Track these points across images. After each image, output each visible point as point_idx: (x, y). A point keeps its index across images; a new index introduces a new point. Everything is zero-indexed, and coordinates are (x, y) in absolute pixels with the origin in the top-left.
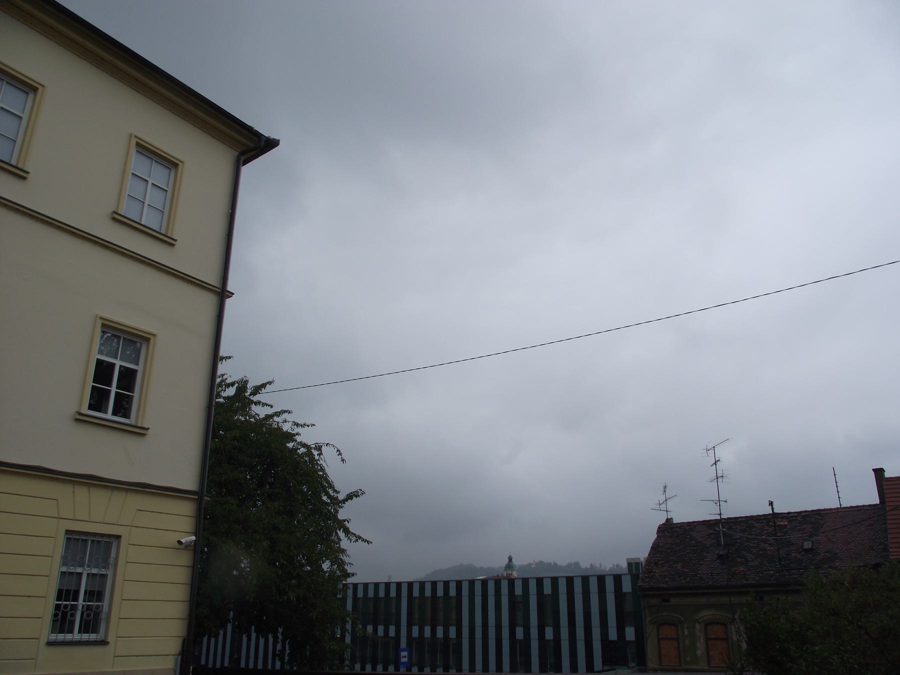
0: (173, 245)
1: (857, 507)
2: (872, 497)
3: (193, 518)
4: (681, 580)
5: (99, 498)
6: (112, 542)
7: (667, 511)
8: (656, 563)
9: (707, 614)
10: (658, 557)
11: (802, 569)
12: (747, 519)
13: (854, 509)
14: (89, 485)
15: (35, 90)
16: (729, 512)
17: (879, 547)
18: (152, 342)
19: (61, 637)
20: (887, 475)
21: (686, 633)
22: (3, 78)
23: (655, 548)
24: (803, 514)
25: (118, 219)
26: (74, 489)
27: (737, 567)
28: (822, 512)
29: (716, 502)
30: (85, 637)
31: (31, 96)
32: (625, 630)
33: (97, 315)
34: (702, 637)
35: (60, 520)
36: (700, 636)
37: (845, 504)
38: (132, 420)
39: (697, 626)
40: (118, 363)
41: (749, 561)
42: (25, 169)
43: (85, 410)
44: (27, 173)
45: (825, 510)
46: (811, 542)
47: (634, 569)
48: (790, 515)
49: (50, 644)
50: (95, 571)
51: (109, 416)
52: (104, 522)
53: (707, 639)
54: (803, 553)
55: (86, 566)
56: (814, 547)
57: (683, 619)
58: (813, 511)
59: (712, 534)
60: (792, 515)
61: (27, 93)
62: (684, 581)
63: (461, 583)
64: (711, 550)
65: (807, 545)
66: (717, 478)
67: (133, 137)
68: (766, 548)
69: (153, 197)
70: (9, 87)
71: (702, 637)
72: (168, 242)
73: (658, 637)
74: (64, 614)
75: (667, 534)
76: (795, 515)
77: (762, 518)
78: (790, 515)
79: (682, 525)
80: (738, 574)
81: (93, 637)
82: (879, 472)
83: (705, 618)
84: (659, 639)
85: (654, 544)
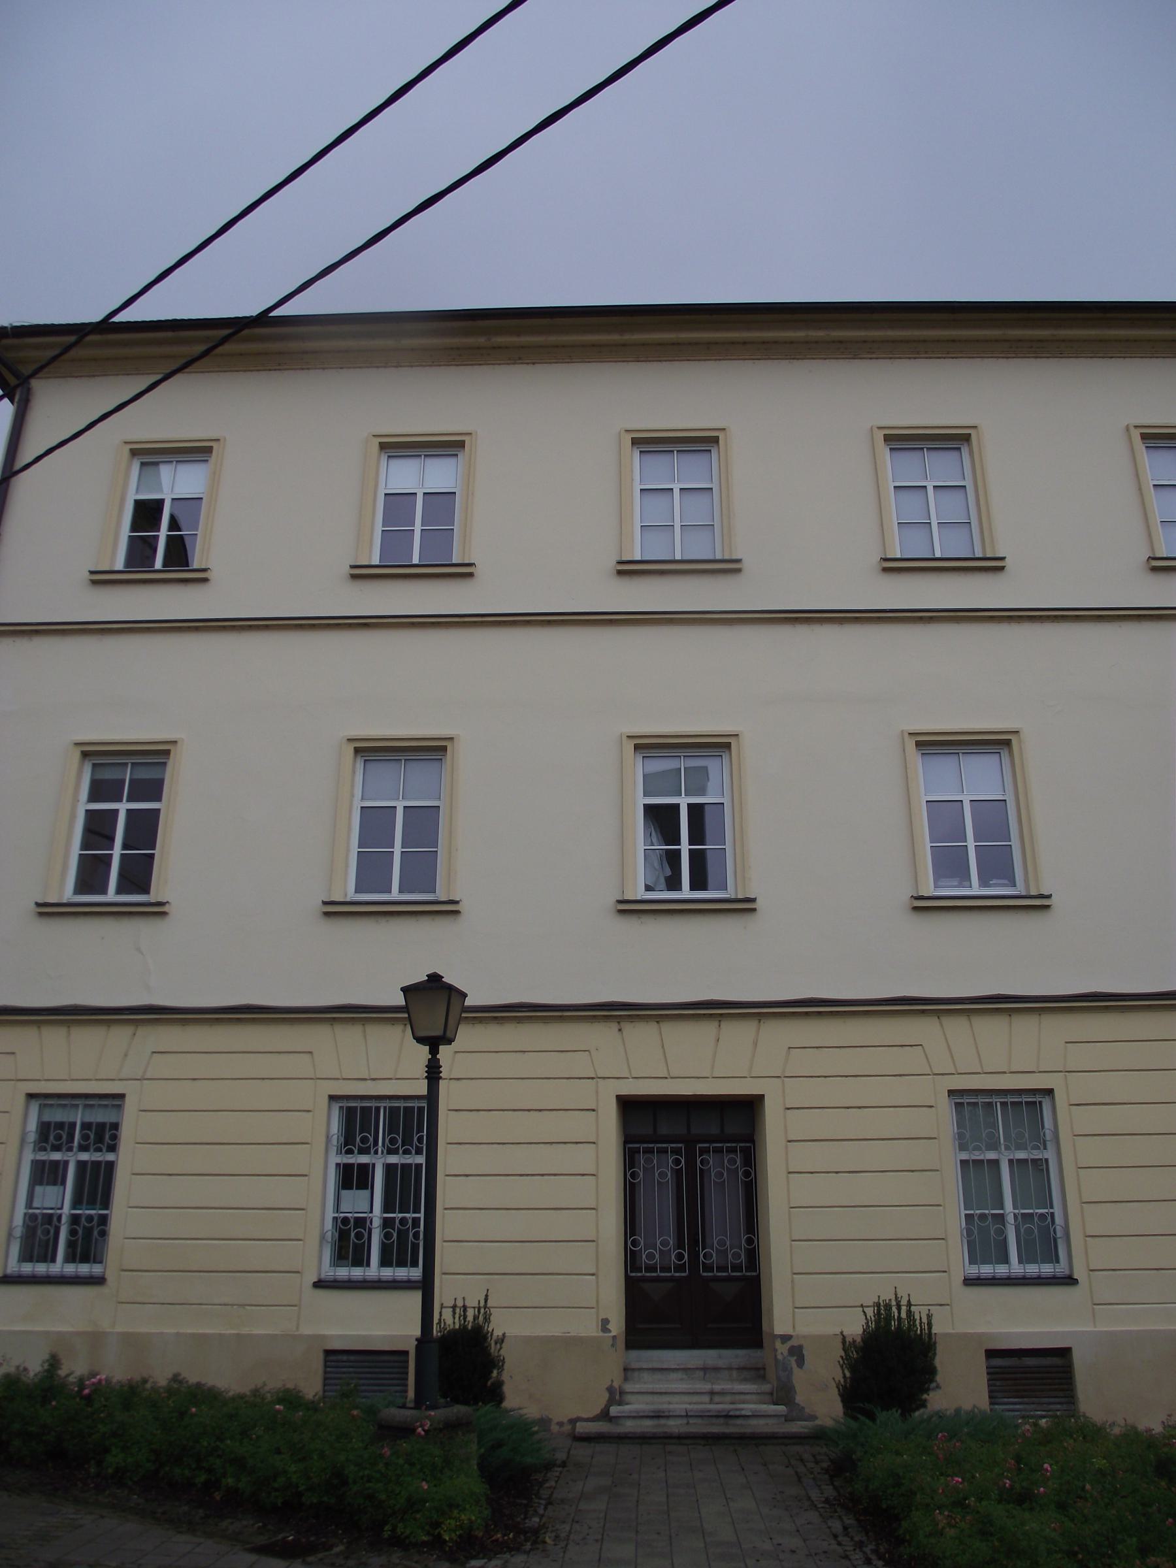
0: (1002, 568)
5: (87, 1039)
6: (1040, 1103)
14: (68, 1024)
15: (967, 438)
18: (1014, 743)
19: (343, 1272)
22: (206, 459)
25: (628, 570)
30: (388, 1273)
31: (965, 450)
33: (902, 731)
35: (318, 1081)
38: (152, 897)
40: (683, 802)
42: (734, 557)
43: (929, 889)
44: (738, 561)
49: (969, 1282)
50: (1021, 1155)
51: (686, 892)
52: (18, 1078)
55: (1003, 1147)
61: (457, 455)
67: (1132, 429)
69: (937, 508)
70: (934, 454)
72: (993, 566)
74: (402, 1235)
81: (1047, 1269)
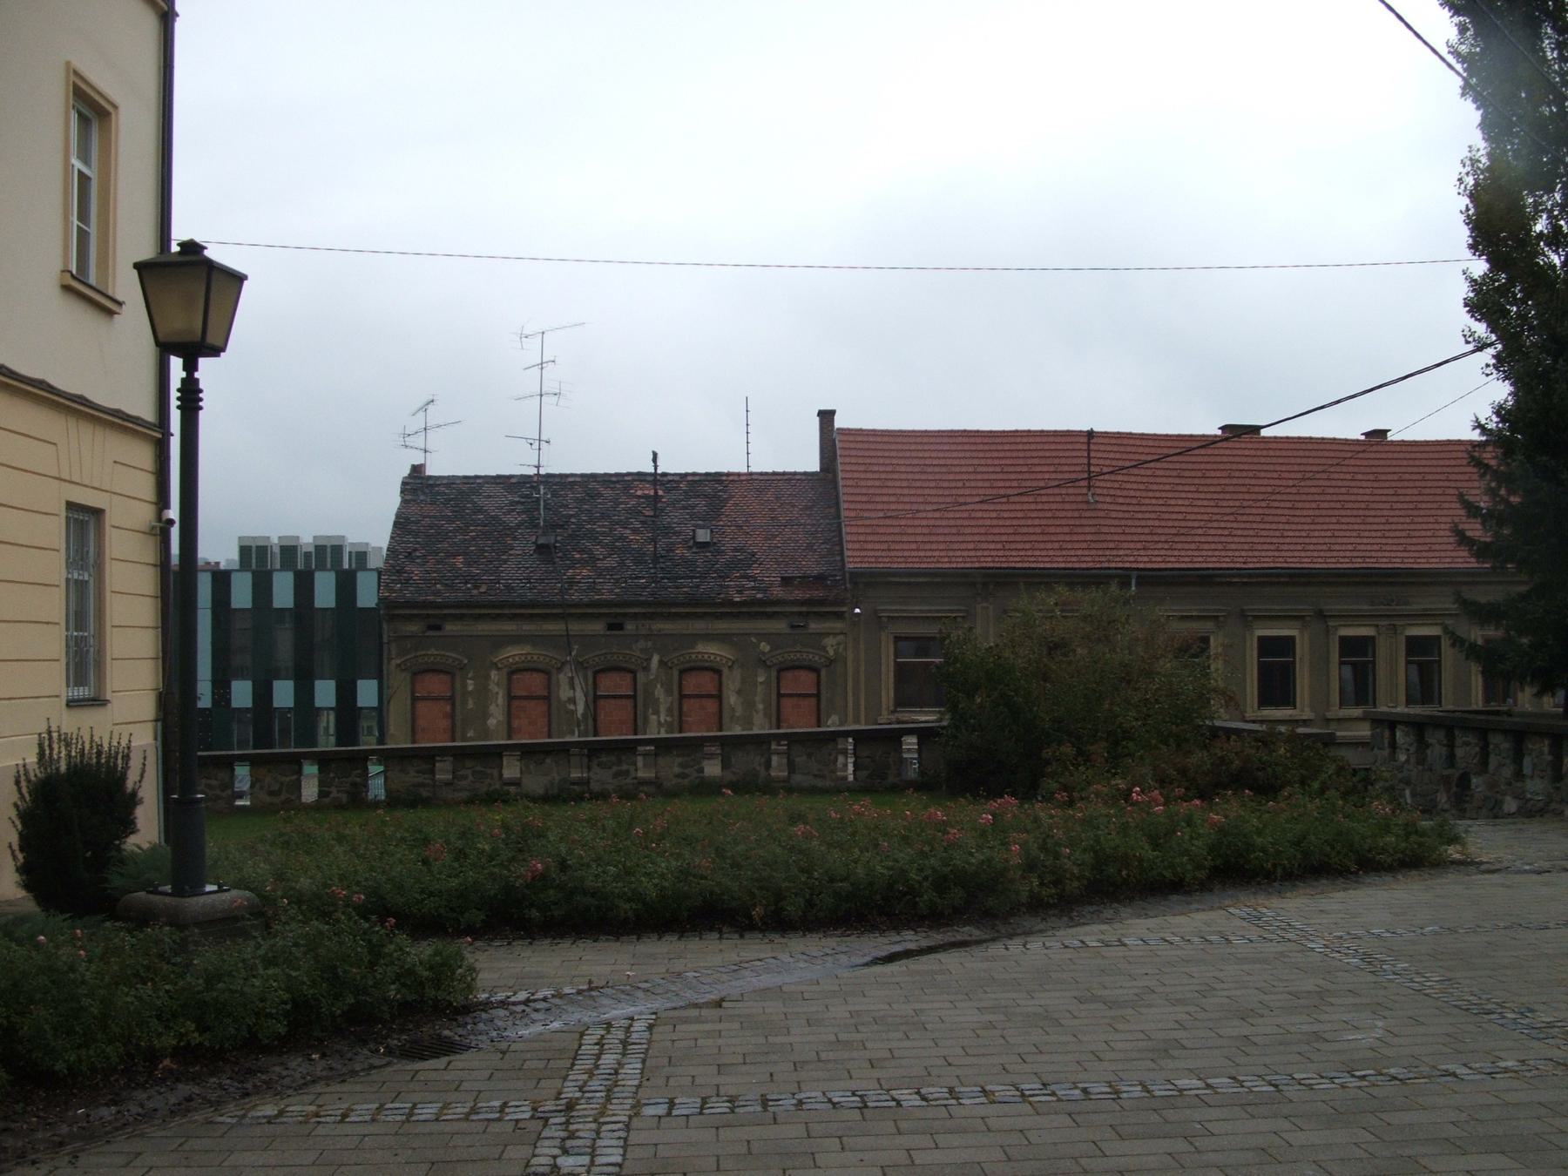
1: (784, 474)
2: (808, 460)
3: (150, 475)
4: (469, 589)
7: (426, 451)
8: (410, 553)
9: (513, 653)
10: (411, 542)
11: (697, 578)
12: (585, 479)
13: (779, 478)
16: (559, 463)
17: (823, 546)
20: (840, 422)
21: (470, 688)
23: (402, 524)
24: (690, 478)
26: (94, 434)
27: (577, 568)
28: (724, 478)
29: (532, 442)
32: (230, 688)
34: (500, 695)
36: (497, 693)
37: (753, 469)
39: (494, 674)
41: (599, 559)
45: (729, 474)
46: (709, 531)
47: (329, 560)
48: (665, 479)
53: (511, 698)
54: (694, 550)
56: (715, 541)
57: (466, 661)
58: (707, 474)
59: (518, 502)
60: (670, 478)
62: (475, 592)
63: (230, 576)
64: (521, 534)
65: (703, 535)
66: (541, 395)
68: (627, 537)
71: (500, 695)
73: (413, 693)
75: (422, 497)
76: (677, 478)
77: (614, 479)
78: (665, 479)
79: (450, 481)
80: (579, 582)
82: (826, 417)
83: (511, 660)
84: (415, 699)
85: (398, 516)
